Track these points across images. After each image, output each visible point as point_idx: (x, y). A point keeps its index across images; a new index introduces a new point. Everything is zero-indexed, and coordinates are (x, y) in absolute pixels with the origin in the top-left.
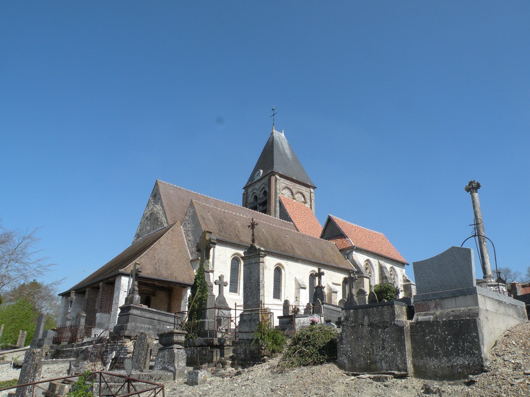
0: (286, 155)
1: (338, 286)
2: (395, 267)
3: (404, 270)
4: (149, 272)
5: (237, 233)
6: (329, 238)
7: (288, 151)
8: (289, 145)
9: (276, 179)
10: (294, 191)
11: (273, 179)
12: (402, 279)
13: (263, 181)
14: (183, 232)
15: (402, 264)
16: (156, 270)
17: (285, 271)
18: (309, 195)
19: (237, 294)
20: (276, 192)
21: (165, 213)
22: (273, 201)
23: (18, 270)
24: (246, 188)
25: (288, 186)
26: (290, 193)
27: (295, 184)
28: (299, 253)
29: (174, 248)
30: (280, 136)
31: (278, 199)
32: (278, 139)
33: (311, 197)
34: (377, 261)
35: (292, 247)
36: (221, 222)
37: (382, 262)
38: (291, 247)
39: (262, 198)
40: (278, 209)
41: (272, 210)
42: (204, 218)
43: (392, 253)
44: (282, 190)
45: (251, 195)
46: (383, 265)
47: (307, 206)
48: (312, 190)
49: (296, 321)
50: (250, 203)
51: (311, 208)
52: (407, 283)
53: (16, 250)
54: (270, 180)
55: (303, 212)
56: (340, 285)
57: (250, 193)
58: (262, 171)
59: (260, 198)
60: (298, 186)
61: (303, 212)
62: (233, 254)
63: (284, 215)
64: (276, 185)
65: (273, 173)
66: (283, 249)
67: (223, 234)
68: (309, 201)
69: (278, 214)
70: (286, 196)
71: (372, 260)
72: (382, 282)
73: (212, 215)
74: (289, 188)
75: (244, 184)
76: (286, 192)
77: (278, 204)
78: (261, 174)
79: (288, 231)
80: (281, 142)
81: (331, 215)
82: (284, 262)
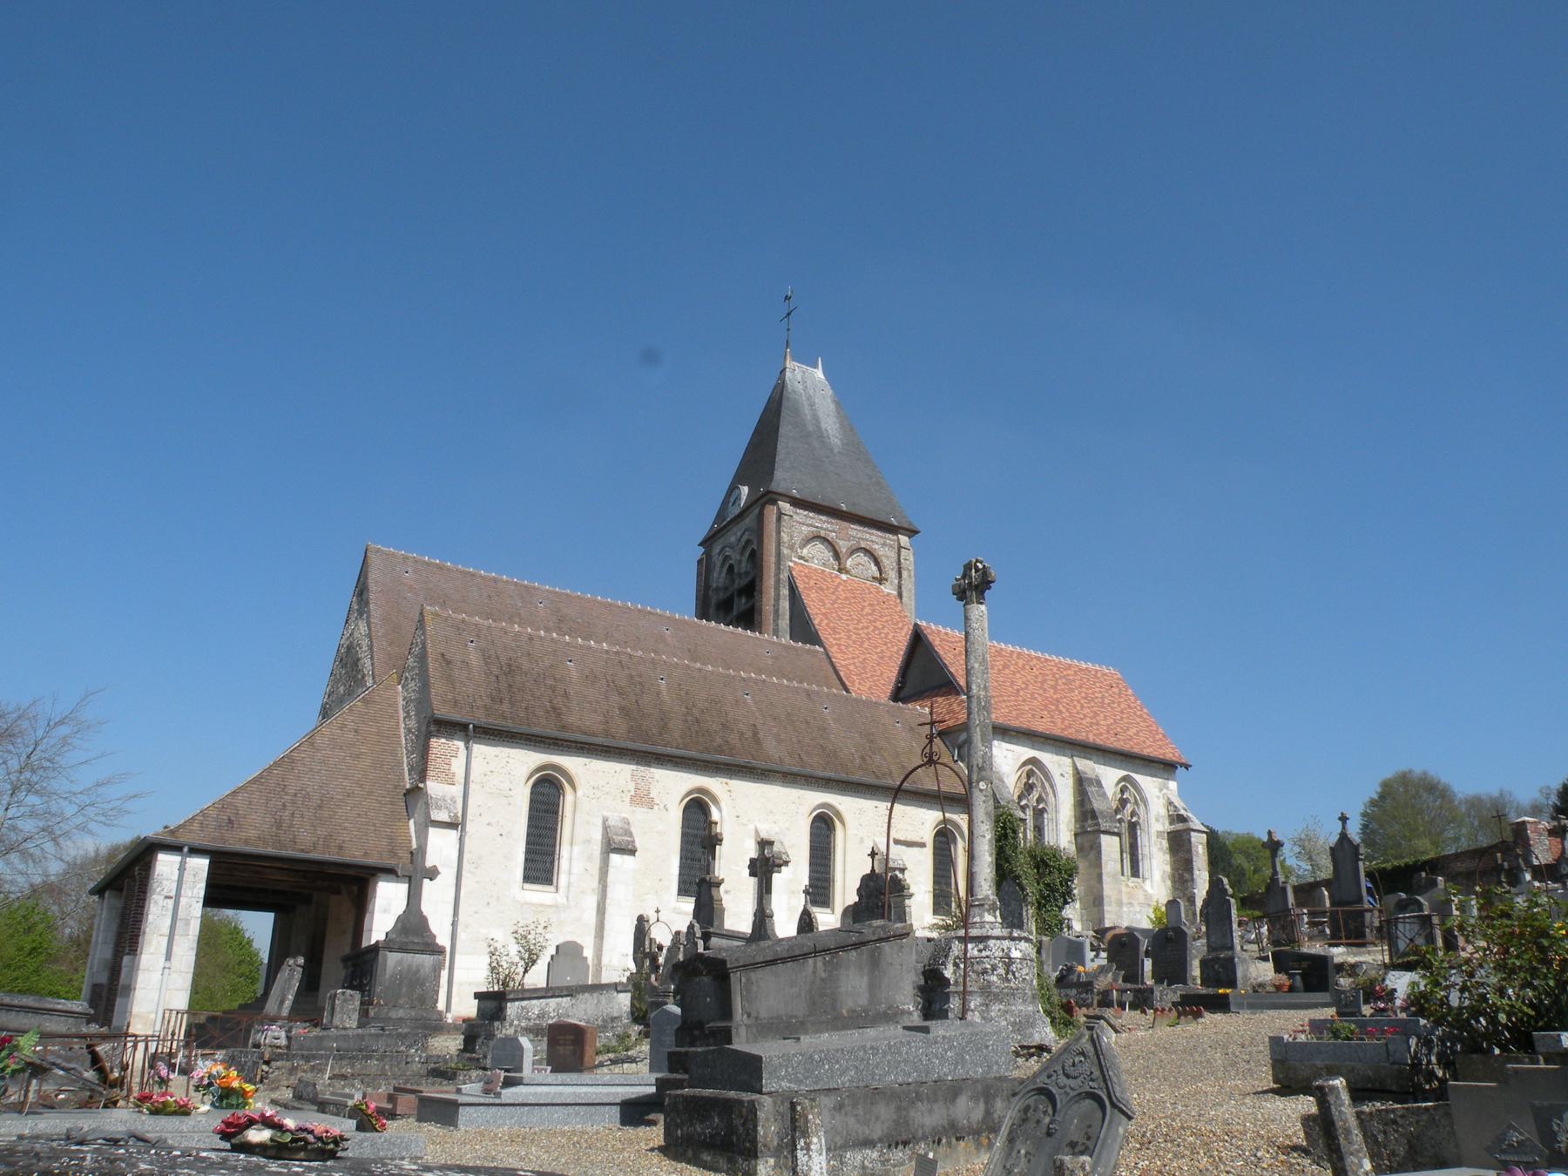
0: (821, 436)
1: (915, 850)
2: (1138, 778)
3: (1173, 785)
4: (253, 834)
5: (558, 701)
6: (905, 700)
7: (830, 423)
8: (838, 404)
9: (780, 514)
10: (843, 546)
11: (771, 512)
12: (1163, 812)
13: (747, 521)
14: (401, 703)
15: (1166, 767)
16: (279, 827)
17: (720, 810)
18: (893, 554)
19: (552, 888)
20: (779, 554)
21: (371, 647)
22: (769, 581)
23: (33, 814)
24: (707, 542)
25: (823, 533)
26: (829, 555)
27: (846, 524)
28: (774, 751)
29: (358, 756)
30: (809, 380)
31: (784, 576)
32: (800, 387)
33: (899, 563)
34: (1067, 761)
35: (755, 734)
36: (511, 669)
37: (1088, 766)
38: (749, 734)
39: (747, 573)
40: (785, 605)
41: (768, 606)
42: (448, 663)
43: (1132, 732)
44: (800, 549)
45: (719, 564)
46: (1090, 775)
47: (889, 589)
48: (904, 539)
49: (509, 1012)
50: (717, 589)
51: (900, 595)
52: (1180, 826)
53: (33, 758)
54: (760, 518)
55: (867, 610)
56: (923, 845)
57: (717, 560)
58: (745, 490)
59: (739, 575)
60: (855, 530)
61: (867, 610)
62: (533, 766)
63: (803, 629)
64: (779, 533)
65: (771, 498)
66: (719, 741)
67: (506, 707)
68: (892, 575)
69: (785, 622)
70: (814, 565)
71: (1048, 758)
72: (1082, 827)
73: (483, 651)
74: (825, 540)
75: (702, 534)
76: (818, 552)
77: (785, 592)
78: (744, 498)
79: (756, 682)
80: (809, 398)
81: (923, 624)
82: (714, 784)
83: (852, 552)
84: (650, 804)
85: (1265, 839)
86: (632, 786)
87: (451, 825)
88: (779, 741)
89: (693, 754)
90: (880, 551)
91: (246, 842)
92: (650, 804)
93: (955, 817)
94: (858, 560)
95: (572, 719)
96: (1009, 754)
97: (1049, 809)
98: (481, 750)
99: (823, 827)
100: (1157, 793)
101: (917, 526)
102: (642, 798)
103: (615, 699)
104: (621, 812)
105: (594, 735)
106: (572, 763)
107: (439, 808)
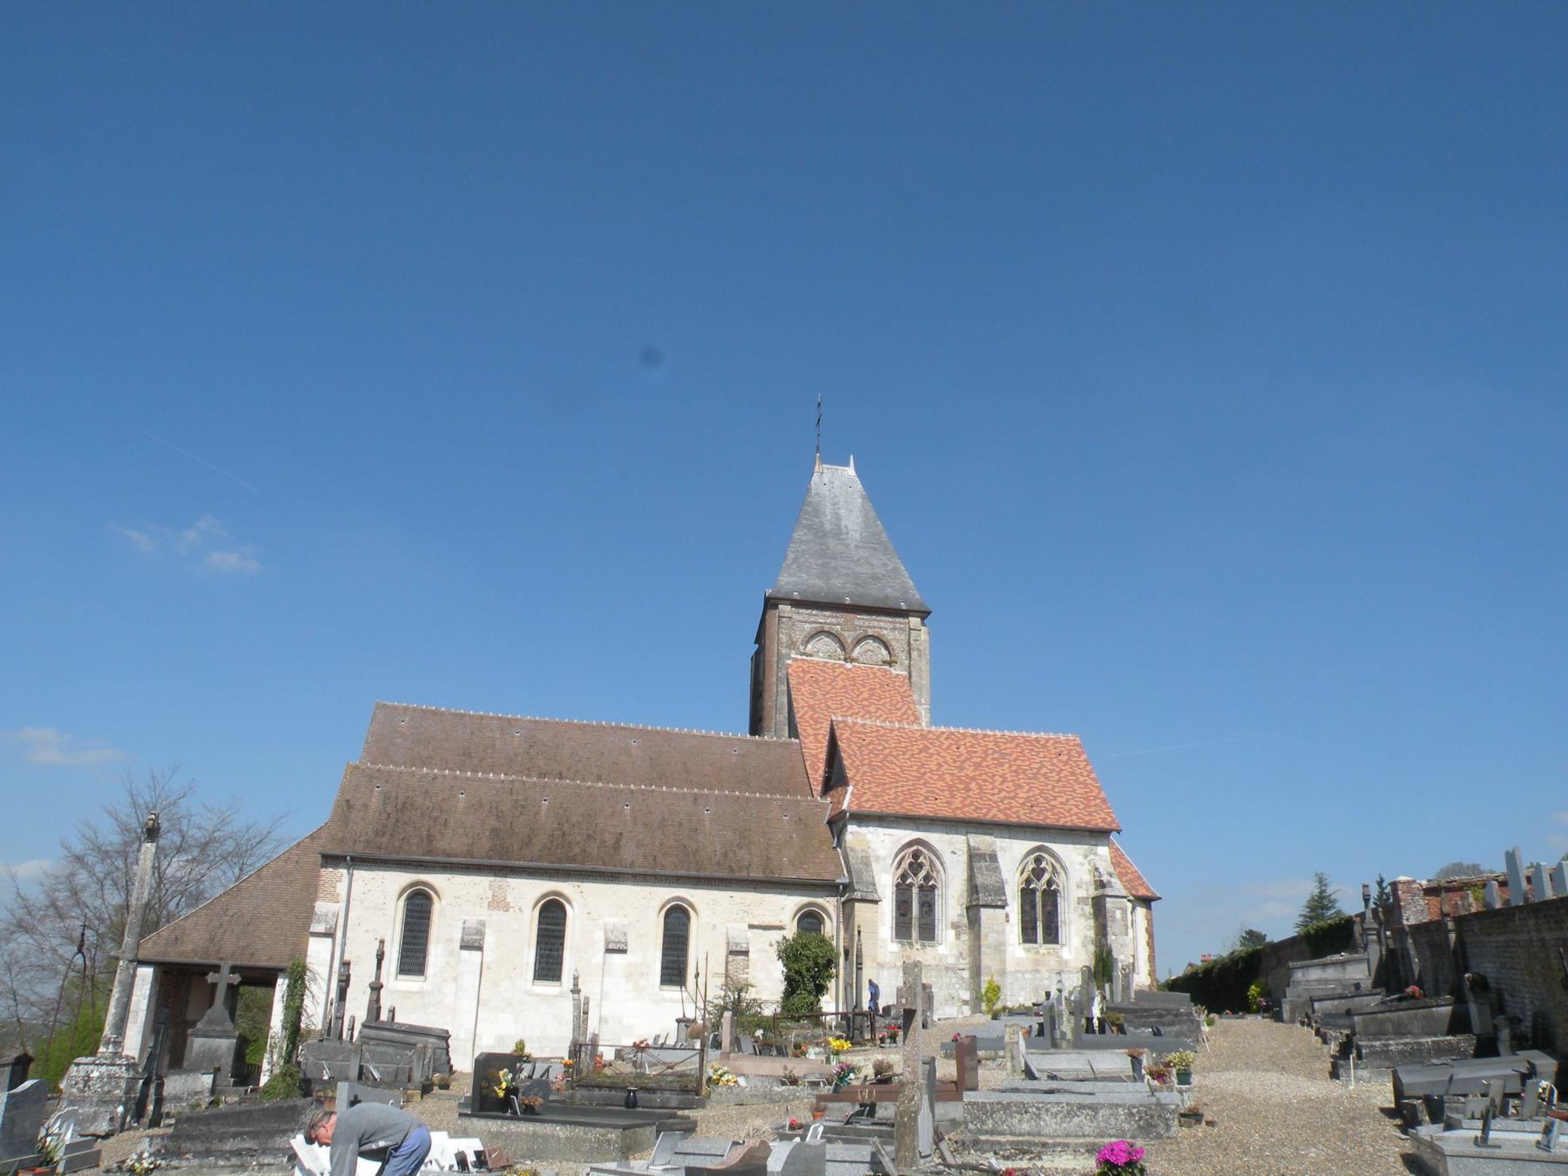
2: (1056, 847)
3: (1103, 851)
10: (849, 637)
15: (1098, 835)
18: (903, 637)
25: (826, 628)
33: (909, 644)
35: (618, 841)
37: (982, 841)
38: (610, 841)
48: (915, 621)
60: (862, 620)
66: (577, 850)
68: (903, 656)
71: (934, 838)
74: (829, 634)
76: (824, 645)
79: (643, 793)
82: (567, 888)
84: (507, 907)
85: (1500, 868)
86: (490, 894)
87: (329, 934)
88: (639, 845)
89: (545, 865)
90: (888, 634)
91: (181, 954)
92: (507, 907)
93: (820, 901)
95: (441, 844)
97: (939, 885)
98: (361, 875)
100: (1077, 867)
101: (929, 606)
102: (499, 904)
103: (493, 822)
104: (476, 913)
106: (436, 879)
107: (319, 922)
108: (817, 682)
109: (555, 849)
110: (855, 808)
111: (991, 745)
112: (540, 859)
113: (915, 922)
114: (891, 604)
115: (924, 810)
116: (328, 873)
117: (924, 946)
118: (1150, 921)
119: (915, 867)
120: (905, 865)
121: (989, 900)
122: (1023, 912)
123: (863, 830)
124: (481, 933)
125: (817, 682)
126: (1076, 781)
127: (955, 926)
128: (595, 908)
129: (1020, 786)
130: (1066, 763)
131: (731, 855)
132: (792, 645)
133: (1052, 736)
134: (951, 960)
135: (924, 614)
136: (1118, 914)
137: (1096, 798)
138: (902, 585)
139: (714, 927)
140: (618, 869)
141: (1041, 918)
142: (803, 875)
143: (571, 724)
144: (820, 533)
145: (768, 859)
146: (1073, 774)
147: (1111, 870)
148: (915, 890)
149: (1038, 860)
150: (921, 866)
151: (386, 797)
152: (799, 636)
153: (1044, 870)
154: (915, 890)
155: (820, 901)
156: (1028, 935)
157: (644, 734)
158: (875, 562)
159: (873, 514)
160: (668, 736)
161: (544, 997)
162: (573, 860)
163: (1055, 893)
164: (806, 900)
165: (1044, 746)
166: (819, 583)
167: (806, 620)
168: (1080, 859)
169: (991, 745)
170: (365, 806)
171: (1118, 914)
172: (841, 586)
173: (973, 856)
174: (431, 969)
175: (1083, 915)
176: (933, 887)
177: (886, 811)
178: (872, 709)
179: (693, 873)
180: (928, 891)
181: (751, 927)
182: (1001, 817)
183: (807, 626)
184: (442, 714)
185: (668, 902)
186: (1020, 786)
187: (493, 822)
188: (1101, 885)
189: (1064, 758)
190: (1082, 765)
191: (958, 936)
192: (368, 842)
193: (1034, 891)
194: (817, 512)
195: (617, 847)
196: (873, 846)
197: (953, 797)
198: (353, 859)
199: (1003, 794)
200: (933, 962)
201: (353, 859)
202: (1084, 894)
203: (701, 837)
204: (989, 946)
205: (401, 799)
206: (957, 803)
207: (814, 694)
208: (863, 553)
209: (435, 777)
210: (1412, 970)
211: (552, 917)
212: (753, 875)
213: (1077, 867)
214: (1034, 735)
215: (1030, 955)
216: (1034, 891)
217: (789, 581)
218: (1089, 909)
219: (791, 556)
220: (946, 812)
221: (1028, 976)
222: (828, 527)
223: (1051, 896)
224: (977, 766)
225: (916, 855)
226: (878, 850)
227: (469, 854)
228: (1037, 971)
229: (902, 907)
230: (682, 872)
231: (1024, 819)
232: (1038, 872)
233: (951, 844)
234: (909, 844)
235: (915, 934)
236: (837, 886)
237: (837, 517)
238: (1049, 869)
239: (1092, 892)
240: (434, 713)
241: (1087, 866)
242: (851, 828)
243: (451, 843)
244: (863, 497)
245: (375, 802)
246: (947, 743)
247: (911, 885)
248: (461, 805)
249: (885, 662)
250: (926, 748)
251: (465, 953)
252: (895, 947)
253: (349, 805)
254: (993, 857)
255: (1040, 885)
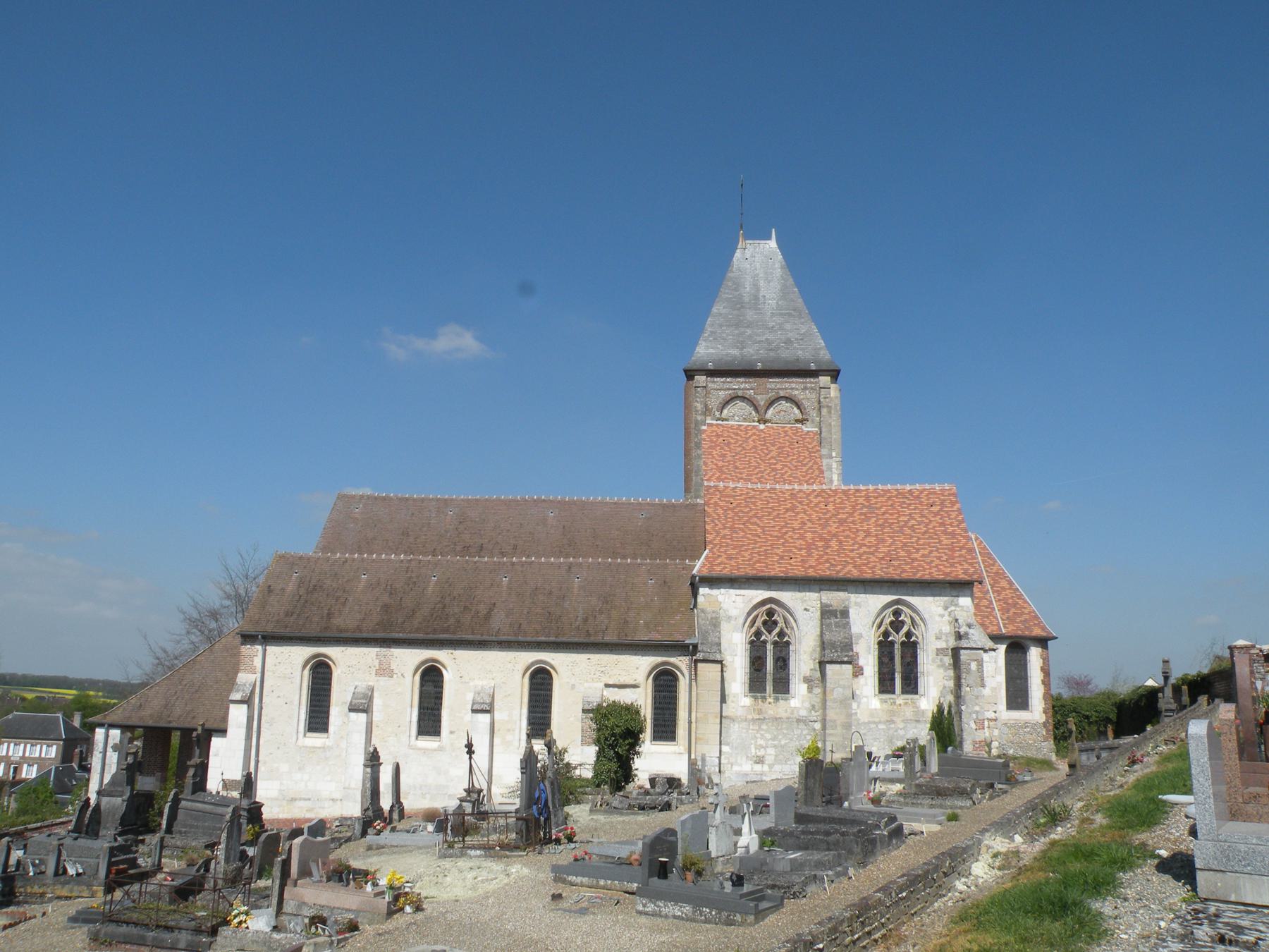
3: (965, 601)
10: (762, 400)
19: (325, 735)
26: (748, 409)
33: (819, 402)
35: (491, 610)
37: (834, 598)
38: (483, 609)
60: (774, 384)
68: (814, 414)
71: (786, 597)
74: (743, 398)
76: (739, 410)
82: (442, 655)
83: (771, 404)
86: (376, 663)
92: (391, 674)
93: (672, 660)
94: (780, 407)
95: (338, 621)
96: (739, 599)
97: (792, 641)
99: (541, 682)
100: (935, 617)
101: (839, 365)
102: (384, 671)
104: (365, 680)
105: (347, 631)
106: (333, 652)
107: (238, 691)
108: (729, 444)
109: (431, 622)
110: (705, 573)
111: (861, 500)
112: (417, 630)
113: (769, 678)
114: (802, 367)
115: (776, 571)
116: (247, 649)
117: (777, 699)
118: (1046, 660)
119: (770, 624)
120: (759, 623)
121: (835, 656)
122: (881, 663)
123: (715, 592)
124: (371, 699)
125: (729, 444)
126: (945, 532)
127: (807, 680)
128: (466, 672)
129: (883, 541)
130: (936, 514)
131: (591, 620)
132: (707, 411)
133: (927, 486)
134: (803, 713)
135: (835, 374)
136: (974, 666)
137: (962, 548)
138: (810, 343)
139: (573, 686)
140: (485, 637)
141: (899, 667)
142: (655, 636)
143: (499, 500)
144: (738, 304)
145: (626, 622)
146: (942, 524)
147: (972, 620)
148: (769, 647)
149: (897, 613)
150: (775, 623)
151: (301, 581)
152: (714, 403)
153: (903, 623)
154: (769, 647)
155: (672, 660)
156: (885, 685)
157: (562, 504)
158: (788, 327)
159: (791, 281)
160: (583, 505)
161: (425, 750)
162: (446, 630)
163: (915, 644)
164: (659, 659)
165: (918, 497)
166: (735, 352)
167: (721, 388)
168: (941, 610)
169: (861, 500)
170: (283, 589)
171: (974, 666)
172: (754, 353)
173: (827, 613)
174: (331, 728)
175: (942, 666)
176: (788, 643)
177: (736, 573)
178: (778, 466)
179: (552, 639)
180: (783, 648)
181: (607, 686)
182: (855, 574)
183: (722, 393)
184: (391, 499)
185: (533, 664)
186: (883, 541)
187: (385, 599)
188: (959, 636)
189: (935, 509)
190: (954, 515)
191: (810, 690)
192: (278, 621)
193: (892, 643)
194: (738, 285)
195: (488, 616)
196: (724, 606)
197: (810, 555)
198: (264, 637)
199: (864, 549)
200: (784, 715)
201: (264, 637)
202: (944, 645)
203: (566, 605)
204: (835, 701)
205: (313, 582)
206: (812, 561)
207: (723, 456)
208: (779, 320)
209: (346, 561)
210: (1165, 794)
211: (431, 678)
212: (608, 639)
213: (935, 617)
214: (908, 487)
215: (885, 706)
216: (892, 643)
217: (706, 351)
218: (948, 660)
219: (708, 329)
220: (799, 572)
221: (881, 726)
222: (746, 299)
223: (911, 647)
224: (842, 522)
225: (770, 613)
226: (731, 610)
227: (359, 628)
228: (892, 722)
229: (757, 663)
230: (543, 639)
231: (879, 574)
232: (897, 625)
233: (803, 601)
234: (763, 603)
235: (769, 688)
236: (687, 646)
237: (756, 287)
238: (908, 621)
239: (952, 643)
240: (384, 499)
241: (947, 618)
242: (703, 591)
243: (346, 620)
244: (782, 268)
245: (291, 586)
246: (816, 501)
247: (765, 642)
248: (363, 584)
249: (797, 421)
250: (794, 507)
251: (353, 715)
252: (747, 701)
253: (270, 590)
254: (845, 613)
255: (898, 638)
